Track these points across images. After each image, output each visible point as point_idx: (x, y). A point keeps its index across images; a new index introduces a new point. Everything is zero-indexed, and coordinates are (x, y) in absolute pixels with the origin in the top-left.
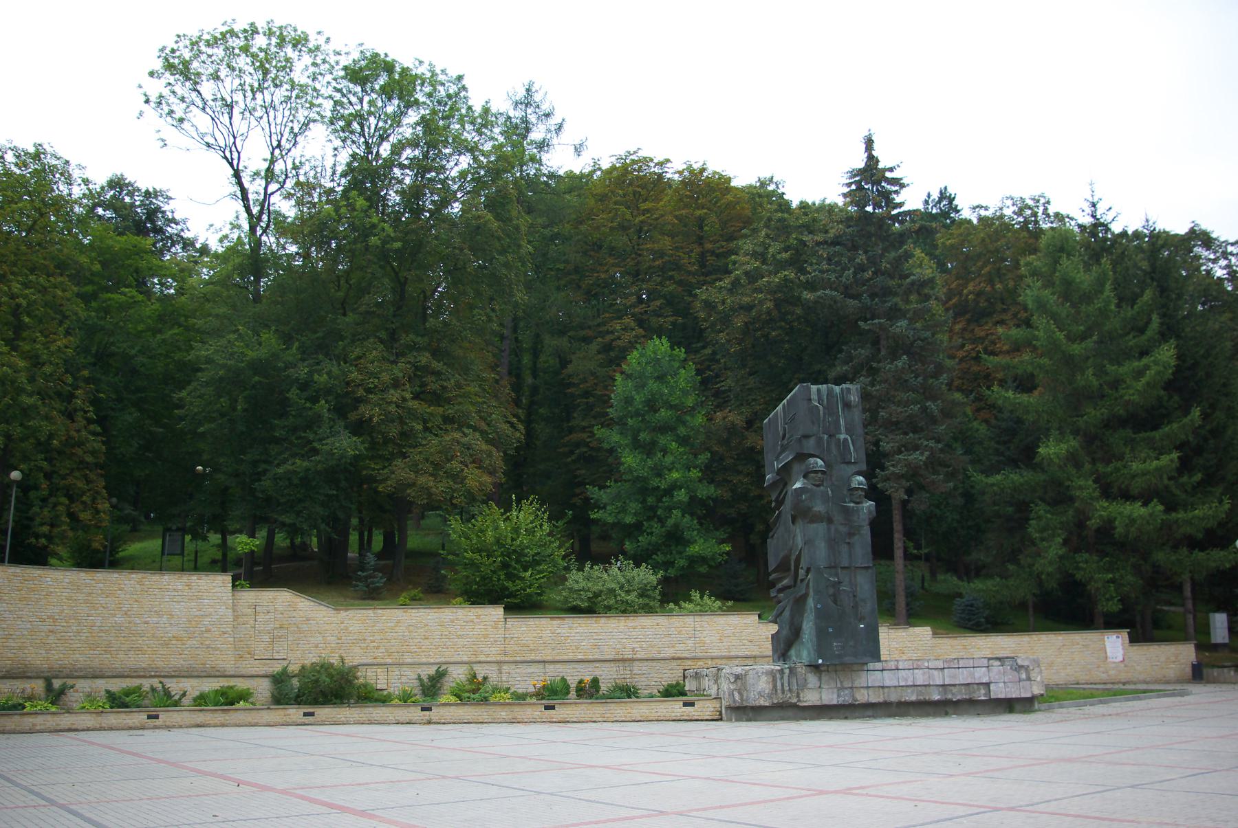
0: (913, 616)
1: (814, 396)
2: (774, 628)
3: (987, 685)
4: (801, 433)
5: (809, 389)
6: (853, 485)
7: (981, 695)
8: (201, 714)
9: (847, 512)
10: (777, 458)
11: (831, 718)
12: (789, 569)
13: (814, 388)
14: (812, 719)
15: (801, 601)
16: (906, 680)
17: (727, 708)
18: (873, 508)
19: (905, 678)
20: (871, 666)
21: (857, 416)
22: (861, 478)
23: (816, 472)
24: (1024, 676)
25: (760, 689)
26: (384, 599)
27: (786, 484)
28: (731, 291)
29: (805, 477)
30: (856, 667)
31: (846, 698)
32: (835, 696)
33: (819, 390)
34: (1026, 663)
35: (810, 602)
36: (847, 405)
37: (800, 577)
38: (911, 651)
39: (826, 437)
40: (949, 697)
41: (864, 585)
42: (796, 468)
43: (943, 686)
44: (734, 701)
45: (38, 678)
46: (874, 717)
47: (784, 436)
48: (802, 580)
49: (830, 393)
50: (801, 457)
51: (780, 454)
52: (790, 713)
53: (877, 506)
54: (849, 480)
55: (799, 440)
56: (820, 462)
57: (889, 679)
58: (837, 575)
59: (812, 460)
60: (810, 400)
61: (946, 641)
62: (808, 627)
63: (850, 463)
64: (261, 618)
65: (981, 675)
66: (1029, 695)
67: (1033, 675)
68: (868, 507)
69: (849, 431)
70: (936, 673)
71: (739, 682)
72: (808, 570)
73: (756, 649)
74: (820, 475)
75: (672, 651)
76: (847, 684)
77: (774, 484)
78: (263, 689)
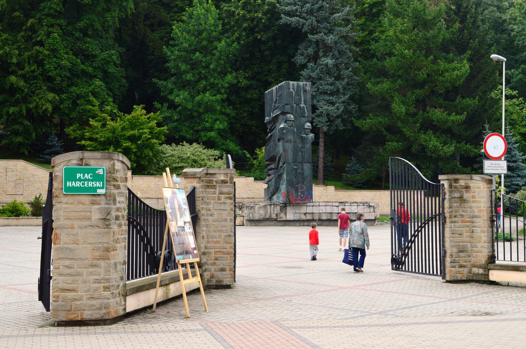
0: (327, 180)
1: (291, 87)
2: (266, 186)
4: (285, 102)
5: (289, 83)
6: (306, 127)
8: (7, 220)
9: (302, 139)
10: (273, 112)
11: (290, 226)
12: (275, 161)
13: (291, 82)
14: (282, 226)
15: (280, 176)
17: (246, 220)
18: (313, 137)
19: (323, 209)
20: (308, 204)
23: (290, 121)
24: (372, 210)
25: (259, 213)
27: (275, 123)
29: (285, 122)
31: (297, 217)
33: (293, 84)
34: (373, 205)
35: (285, 176)
36: (305, 91)
37: (280, 165)
38: (326, 197)
39: (295, 105)
41: (307, 168)
42: (281, 117)
44: (250, 217)
45: (493, 246)
47: (276, 102)
48: (281, 167)
49: (298, 86)
50: (284, 113)
51: (274, 110)
52: (267, 223)
53: (315, 136)
54: (304, 125)
55: (283, 106)
56: (292, 116)
57: (316, 210)
58: (296, 165)
59: (289, 115)
62: (283, 188)
63: (305, 117)
64: (9, 174)
66: (374, 218)
67: (376, 210)
68: (311, 137)
69: (305, 103)
70: (335, 208)
71: (252, 209)
72: (284, 163)
73: (252, 194)
76: (297, 212)
77: (270, 122)
78: (29, 208)
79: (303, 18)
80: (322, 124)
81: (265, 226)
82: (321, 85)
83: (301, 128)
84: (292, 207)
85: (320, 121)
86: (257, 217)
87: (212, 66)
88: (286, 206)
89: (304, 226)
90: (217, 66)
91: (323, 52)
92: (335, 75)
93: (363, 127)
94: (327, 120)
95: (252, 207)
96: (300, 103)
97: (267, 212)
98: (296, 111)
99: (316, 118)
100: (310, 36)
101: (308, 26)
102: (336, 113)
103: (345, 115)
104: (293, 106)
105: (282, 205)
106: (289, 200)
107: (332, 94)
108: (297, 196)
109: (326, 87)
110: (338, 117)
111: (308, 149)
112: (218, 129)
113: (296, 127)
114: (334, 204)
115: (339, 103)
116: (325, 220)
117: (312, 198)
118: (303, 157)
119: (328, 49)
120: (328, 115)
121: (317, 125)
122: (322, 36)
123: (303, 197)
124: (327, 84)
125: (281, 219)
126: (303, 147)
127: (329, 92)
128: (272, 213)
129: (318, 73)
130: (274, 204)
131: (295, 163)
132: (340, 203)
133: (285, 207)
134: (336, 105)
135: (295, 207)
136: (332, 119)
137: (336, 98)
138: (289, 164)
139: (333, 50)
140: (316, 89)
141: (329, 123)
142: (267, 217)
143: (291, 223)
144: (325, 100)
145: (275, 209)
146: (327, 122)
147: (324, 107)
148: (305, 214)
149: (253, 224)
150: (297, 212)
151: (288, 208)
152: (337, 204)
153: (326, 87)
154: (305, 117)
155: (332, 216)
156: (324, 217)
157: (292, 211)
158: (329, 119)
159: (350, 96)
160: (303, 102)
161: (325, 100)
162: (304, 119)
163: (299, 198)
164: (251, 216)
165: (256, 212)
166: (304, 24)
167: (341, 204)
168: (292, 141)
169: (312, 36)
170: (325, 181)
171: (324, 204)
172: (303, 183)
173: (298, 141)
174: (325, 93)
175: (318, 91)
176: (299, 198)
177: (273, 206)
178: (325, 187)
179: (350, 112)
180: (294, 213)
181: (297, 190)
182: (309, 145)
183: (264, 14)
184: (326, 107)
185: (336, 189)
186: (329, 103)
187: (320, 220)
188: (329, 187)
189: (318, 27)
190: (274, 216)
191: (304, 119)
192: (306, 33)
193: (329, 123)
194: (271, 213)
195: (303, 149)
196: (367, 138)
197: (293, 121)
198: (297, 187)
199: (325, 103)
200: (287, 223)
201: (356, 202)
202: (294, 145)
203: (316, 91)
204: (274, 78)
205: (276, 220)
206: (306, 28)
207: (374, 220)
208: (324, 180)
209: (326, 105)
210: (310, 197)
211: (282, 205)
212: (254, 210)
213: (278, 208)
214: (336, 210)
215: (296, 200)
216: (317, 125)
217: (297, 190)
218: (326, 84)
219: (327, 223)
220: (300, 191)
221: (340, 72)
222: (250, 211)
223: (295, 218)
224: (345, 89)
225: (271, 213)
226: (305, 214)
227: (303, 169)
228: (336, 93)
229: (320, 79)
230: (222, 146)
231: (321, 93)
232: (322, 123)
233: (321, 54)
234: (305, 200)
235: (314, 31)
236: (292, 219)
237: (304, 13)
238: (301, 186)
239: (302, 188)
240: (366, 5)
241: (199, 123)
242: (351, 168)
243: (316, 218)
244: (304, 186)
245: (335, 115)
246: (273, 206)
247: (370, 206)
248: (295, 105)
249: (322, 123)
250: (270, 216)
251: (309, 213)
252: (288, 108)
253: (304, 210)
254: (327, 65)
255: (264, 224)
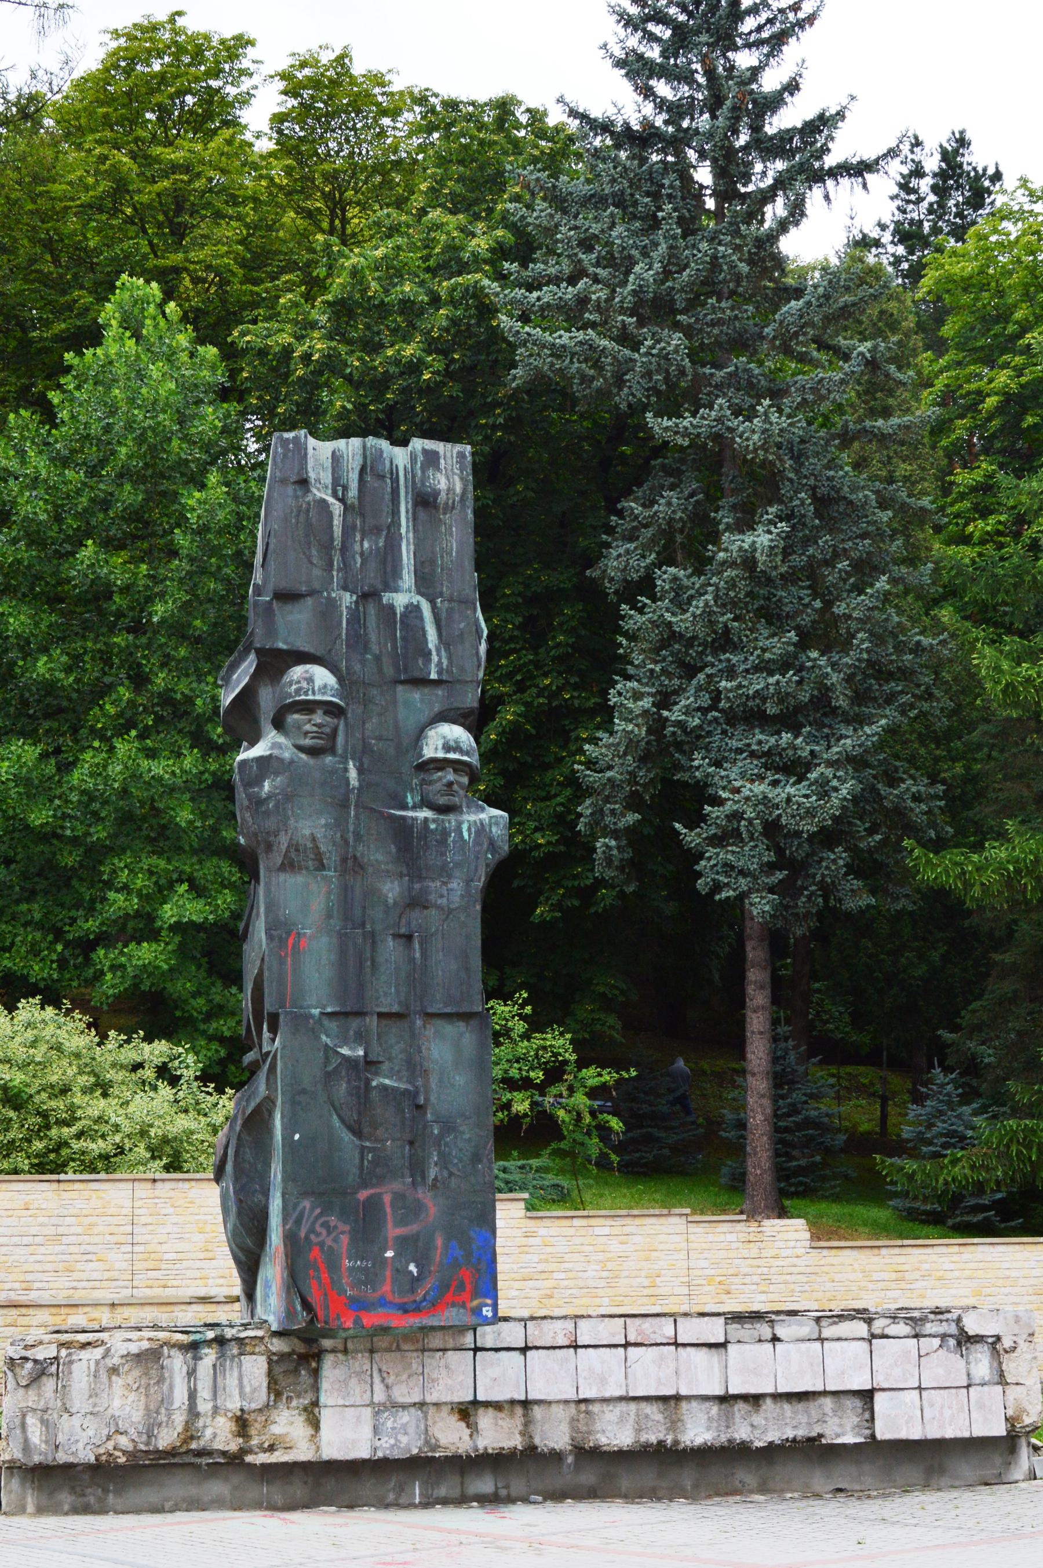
1: (320, 474)
3: (867, 1396)
7: (844, 1430)
9: (408, 841)
13: (320, 451)
14: (273, 1507)
16: (603, 1381)
19: (602, 1374)
20: (488, 1336)
21: (457, 539)
22: (456, 733)
26: (582, 1205)
28: (106, 158)
30: (436, 1340)
31: (402, 1439)
32: (367, 1431)
33: (336, 458)
36: (425, 501)
40: (742, 1432)
43: (725, 1399)
46: (653, 1495)
52: (177, 1487)
56: (322, 676)
57: (549, 1378)
58: (361, 1038)
59: (298, 672)
60: (304, 483)
61: (848, 1257)
63: (423, 682)
65: (846, 1365)
66: (999, 1430)
67: (1012, 1367)
68: (481, 830)
69: (425, 583)
71: (49, 1385)
74: (318, 718)
75: (63, 1282)
79: (625, 338)
80: (743, 883)
81: (157, 1509)
82: (730, 672)
83: (402, 766)
84: (361, 1362)
85: (729, 867)
86: (81, 1441)
87: (159, 610)
88: (318, 1356)
89: (462, 1500)
90: (185, 606)
91: (734, 508)
92: (806, 619)
93: (968, 885)
94: (769, 857)
95: (41, 1371)
96: (390, 579)
97: (166, 1401)
98: (358, 641)
99: (711, 851)
100: (659, 425)
101: (648, 374)
102: (810, 813)
103: (871, 831)
104: (332, 605)
105: (278, 1345)
106: (306, 1305)
107: (789, 719)
108: (369, 1278)
109: (758, 683)
110: (827, 837)
111: (448, 912)
112: (177, 928)
113: (363, 753)
114: (690, 1330)
115: (830, 764)
116: (622, 1456)
117: (491, 1290)
118: (417, 978)
119: (759, 486)
120: (772, 828)
121: (717, 887)
122: (719, 420)
123: (415, 1282)
124: (764, 668)
125: (278, 1457)
126: (416, 902)
127: (771, 709)
128: (204, 1406)
129: (708, 612)
130: (220, 1341)
131: (355, 1024)
132: (736, 1318)
133: (304, 1359)
134: (813, 776)
135: (386, 1361)
136: (797, 850)
137: (811, 739)
138: (301, 1020)
139: (785, 490)
140: (705, 700)
141: (780, 875)
142: (166, 1439)
143: (368, 1487)
144: (753, 754)
145: (231, 1380)
146: (771, 867)
147: (743, 788)
148: (467, 1411)
149: (66, 1498)
150: (403, 1394)
151: (331, 1371)
152: (715, 1330)
153: (758, 683)
154: (423, 682)
155: (674, 1424)
156: (616, 1432)
157: (358, 1392)
158: (780, 852)
159: (978, 847)
160: (408, 579)
161: (753, 754)
162: (416, 696)
163: (386, 1288)
164: (36, 1435)
165: (79, 1401)
166: (623, 368)
167: (745, 1332)
168: (332, 858)
169: (666, 423)
170: (787, 1203)
171: (613, 1332)
172: (417, 1168)
173: (378, 854)
174: (750, 716)
175: (714, 707)
176: (386, 1288)
177: (209, 1356)
178: (753, 1226)
179: (898, 820)
180: (378, 1410)
181: (366, 1224)
182: (456, 885)
183: (432, 346)
184: (759, 788)
185: (820, 1233)
186: (778, 769)
187: (589, 1455)
188: (773, 1226)
189: (699, 381)
190: (218, 1434)
191: (415, 702)
192: (638, 409)
193: (780, 875)
194: (193, 1413)
195: (416, 916)
196: (1007, 958)
197: (331, 709)
198: (373, 1206)
199: (754, 767)
200: (330, 1484)
201: (866, 1316)
202: (346, 890)
203: (704, 711)
204: (510, 675)
205: (235, 1461)
206: (635, 388)
207: (1009, 1443)
208: (783, 1193)
209: (761, 778)
210: (474, 1276)
211: (278, 1345)
212: (62, 1391)
213: (255, 1369)
214: (702, 1375)
215: (361, 1305)
216: (717, 887)
217: (366, 1224)
218: (756, 669)
219: (648, 1476)
220: (393, 1231)
221: (828, 604)
222: (31, 1399)
223: (387, 1447)
224: (860, 697)
225: (193, 1413)
226: (466, 1412)
227: (414, 1067)
228: (816, 712)
229: (724, 641)
230: (209, 1017)
231: (732, 718)
232: (742, 873)
233: (725, 518)
234: (436, 1305)
235: (675, 399)
236: (364, 1453)
237: (622, 311)
238: (399, 1197)
239: (411, 1210)
240: (991, 402)
241: (93, 901)
242: (930, 1126)
243: (554, 1435)
244: (423, 1194)
245: (808, 827)
246: (209, 1356)
247: (965, 1340)
248: (347, 599)
249: (742, 873)
250: (190, 1434)
251: (496, 1406)
252: (294, 626)
253: (452, 1378)
254: (748, 562)
255: (150, 1495)
